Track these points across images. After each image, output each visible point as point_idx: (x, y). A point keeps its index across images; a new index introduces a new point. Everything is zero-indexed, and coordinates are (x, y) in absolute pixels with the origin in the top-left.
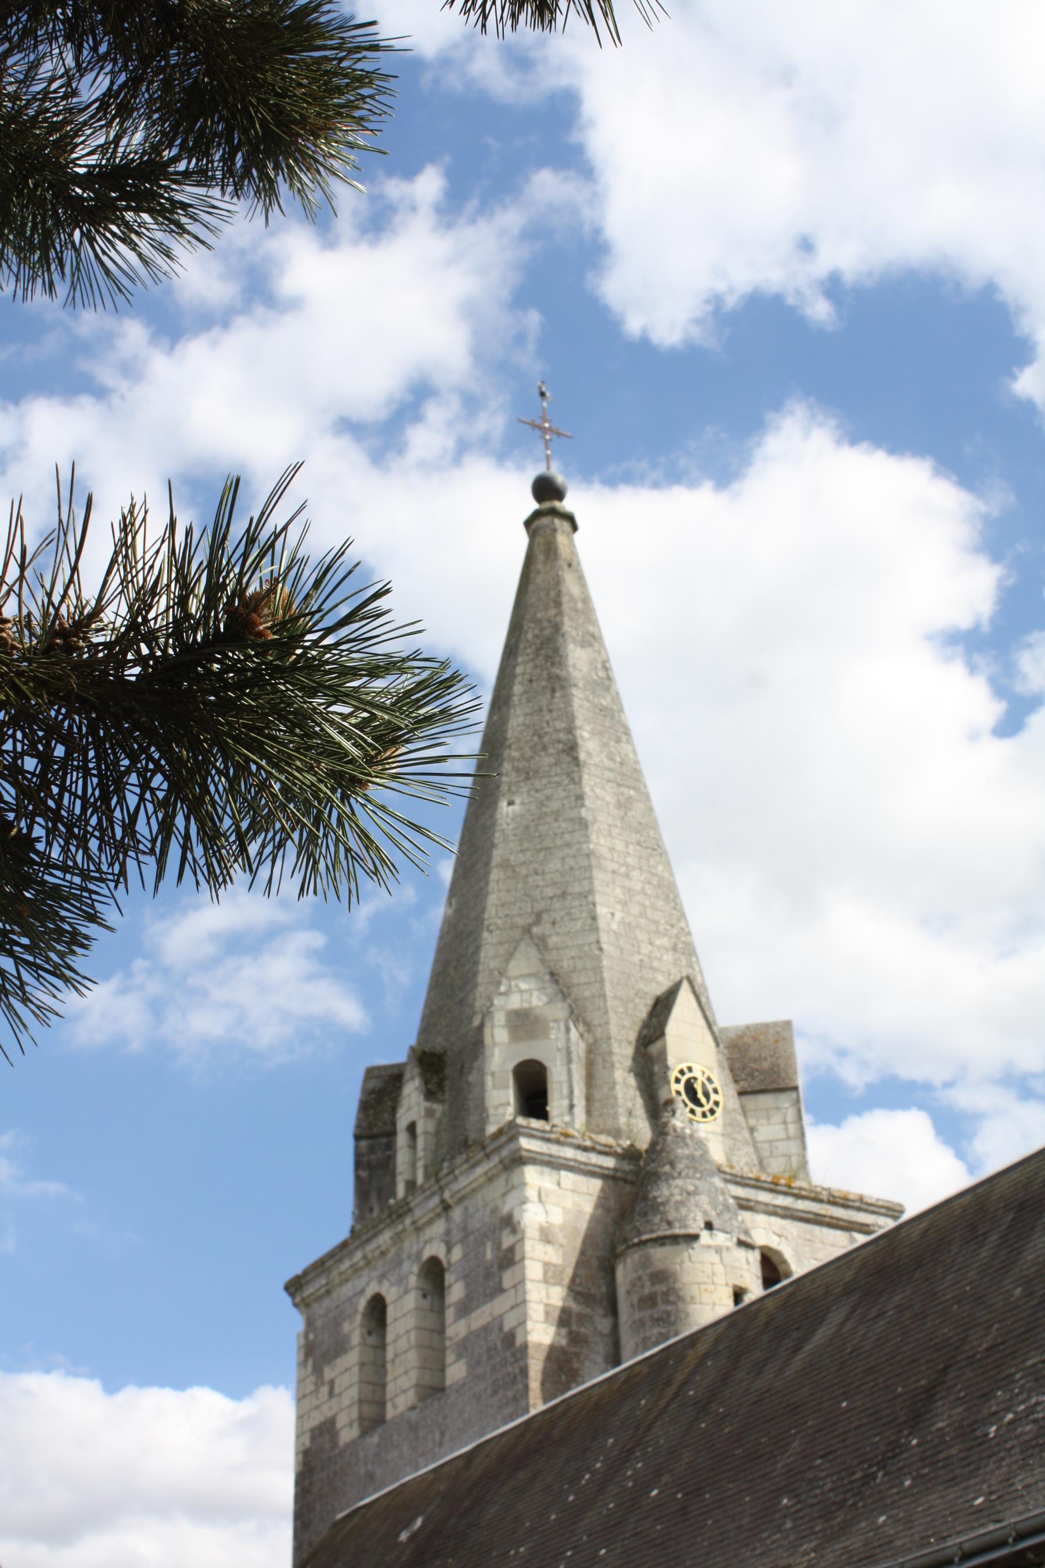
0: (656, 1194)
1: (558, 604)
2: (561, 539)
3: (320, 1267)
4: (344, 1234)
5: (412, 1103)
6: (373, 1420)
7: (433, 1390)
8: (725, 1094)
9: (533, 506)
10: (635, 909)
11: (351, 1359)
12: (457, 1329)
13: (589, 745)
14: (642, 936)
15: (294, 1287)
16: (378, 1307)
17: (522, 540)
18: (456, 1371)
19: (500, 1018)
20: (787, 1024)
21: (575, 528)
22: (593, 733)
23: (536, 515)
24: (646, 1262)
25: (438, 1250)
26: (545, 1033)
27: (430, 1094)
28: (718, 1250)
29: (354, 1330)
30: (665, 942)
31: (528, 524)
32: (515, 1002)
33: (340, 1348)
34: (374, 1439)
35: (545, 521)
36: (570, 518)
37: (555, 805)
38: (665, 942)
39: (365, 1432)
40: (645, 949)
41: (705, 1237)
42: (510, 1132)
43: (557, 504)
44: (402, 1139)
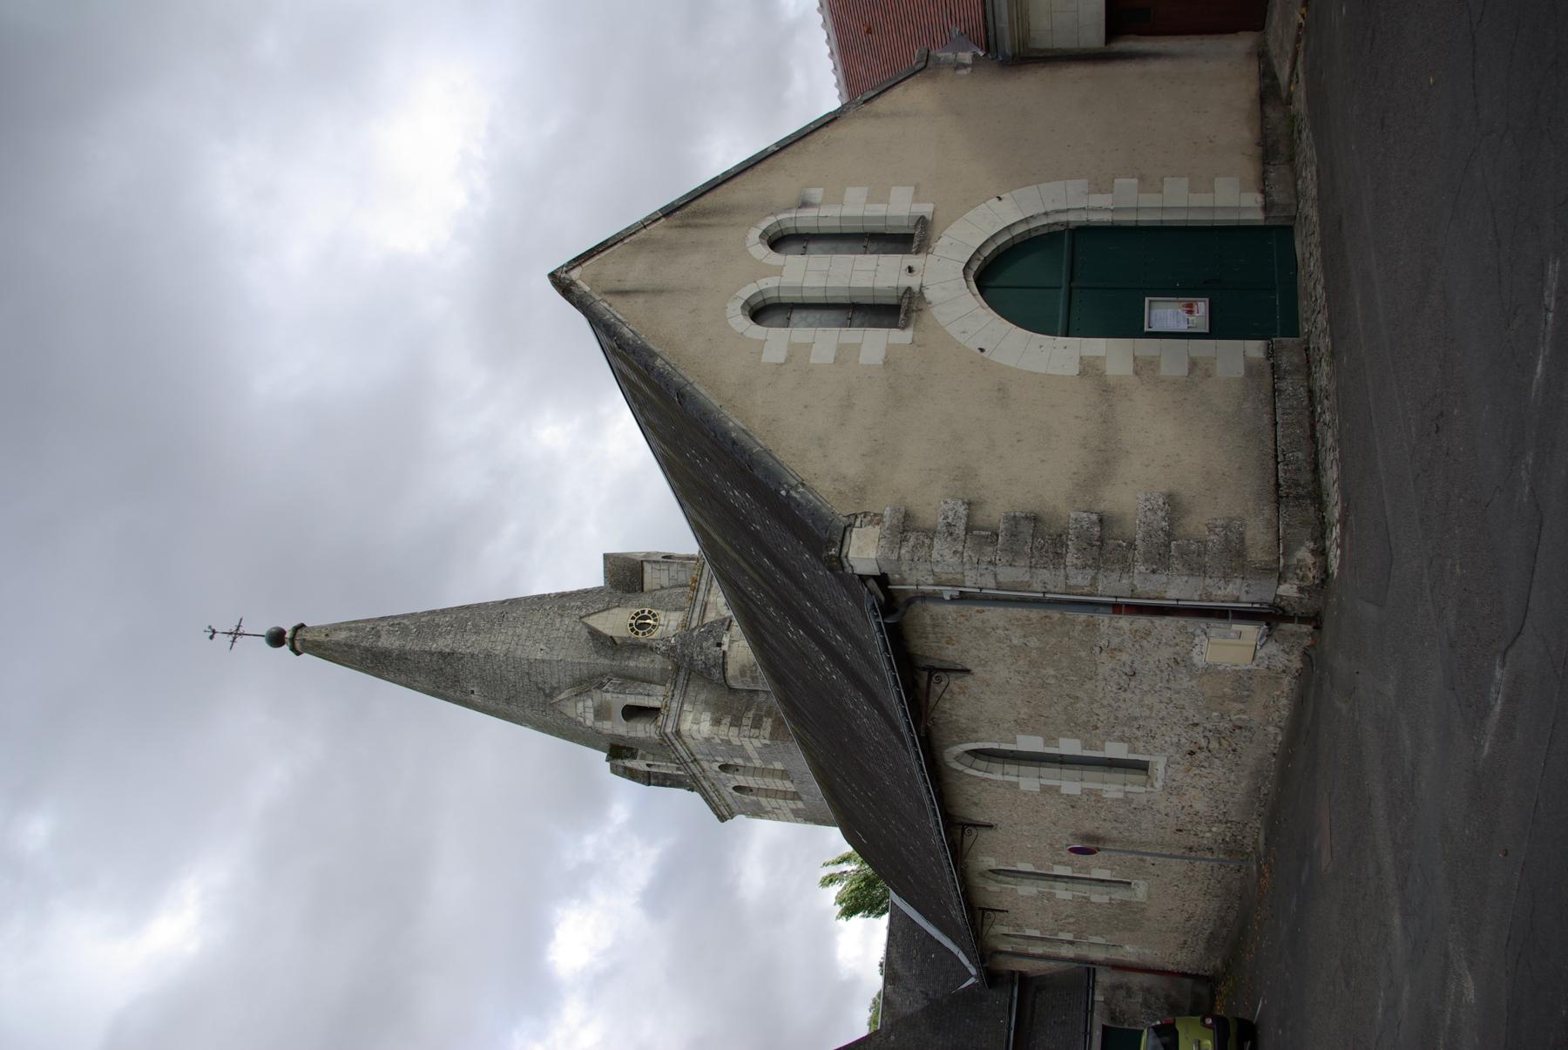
0: (703, 697)
1: (352, 646)
2: (308, 637)
3: (714, 809)
4: (696, 795)
5: (639, 764)
6: (796, 796)
7: (785, 775)
8: (642, 604)
9: (286, 648)
10: (539, 635)
11: (763, 801)
12: (758, 763)
13: (443, 644)
14: (555, 634)
15: (722, 818)
16: (737, 788)
17: (306, 657)
18: (778, 766)
19: (599, 725)
20: (606, 557)
21: (303, 626)
22: (433, 640)
23: (293, 649)
24: (734, 678)
25: (716, 766)
26: (608, 703)
27: (633, 756)
28: (732, 642)
29: (748, 798)
30: (558, 621)
31: (298, 654)
32: (590, 716)
33: (758, 804)
34: (805, 797)
35: (298, 645)
36: (297, 629)
37: (475, 670)
38: (558, 621)
39: (800, 799)
40: (561, 634)
41: (725, 648)
42: (661, 729)
43: (288, 635)
44: (654, 770)
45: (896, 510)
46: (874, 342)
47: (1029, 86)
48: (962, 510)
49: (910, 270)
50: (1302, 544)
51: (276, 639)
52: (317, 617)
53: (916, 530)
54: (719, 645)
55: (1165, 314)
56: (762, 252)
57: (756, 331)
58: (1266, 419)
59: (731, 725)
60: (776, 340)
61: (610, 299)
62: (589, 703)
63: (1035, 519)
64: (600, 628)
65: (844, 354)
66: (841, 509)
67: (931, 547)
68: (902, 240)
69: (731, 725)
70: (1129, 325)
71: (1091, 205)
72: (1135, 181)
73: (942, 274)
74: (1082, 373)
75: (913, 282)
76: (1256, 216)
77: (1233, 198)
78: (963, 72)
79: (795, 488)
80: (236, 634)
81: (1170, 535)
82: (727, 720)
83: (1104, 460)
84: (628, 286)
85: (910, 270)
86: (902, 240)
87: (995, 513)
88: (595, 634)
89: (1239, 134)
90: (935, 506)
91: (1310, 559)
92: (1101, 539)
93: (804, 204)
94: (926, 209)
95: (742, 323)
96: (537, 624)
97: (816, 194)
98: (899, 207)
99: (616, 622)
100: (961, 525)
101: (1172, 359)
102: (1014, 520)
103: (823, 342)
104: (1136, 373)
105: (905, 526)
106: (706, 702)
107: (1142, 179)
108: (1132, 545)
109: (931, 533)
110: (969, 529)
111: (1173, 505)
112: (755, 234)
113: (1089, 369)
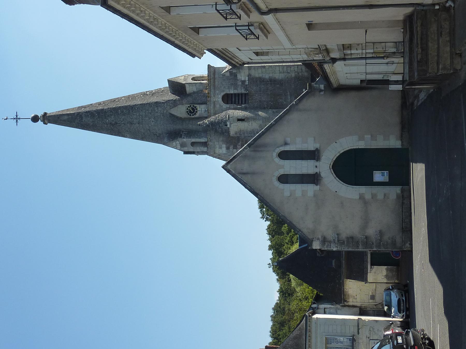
38: (156, 108)
41: (228, 126)
45: (322, 237)
46: (311, 189)
47: (340, 100)
48: (336, 236)
49: (316, 167)
50: (407, 242)
51: (35, 119)
52: (52, 110)
53: (327, 241)
54: (226, 125)
55: (378, 176)
56: (277, 160)
57: (282, 186)
58: (401, 210)
59: (233, 149)
60: (288, 188)
61: (241, 175)
62: (178, 142)
63: (352, 238)
64: (176, 114)
65: (304, 193)
66: (310, 237)
67: (331, 245)
68: (313, 155)
69: (233, 149)
70: (369, 182)
71: (356, 67)
72: (370, 136)
73: (324, 167)
74: (360, 198)
75: (317, 170)
76: (400, 147)
77: (394, 142)
78: (322, 93)
79: (298, 232)
80: (17, 119)
81: (381, 240)
82: (231, 147)
83: (365, 226)
84: (245, 171)
85: (316, 167)
86: (313, 155)
87: (343, 236)
88: (172, 115)
89: (394, 118)
90: (330, 235)
91: (409, 246)
92: (366, 242)
93: (286, 144)
94: (317, 146)
95: (277, 183)
96: (148, 110)
97: (288, 140)
98: (311, 146)
99: (181, 111)
100: (336, 239)
101: (380, 191)
102: (348, 238)
103: (298, 189)
104: (372, 198)
105: (324, 240)
106: (223, 141)
107: (372, 136)
108: (373, 244)
109: (330, 242)
110: (338, 241)
111: (381, 233)
112: (275, 154)
113: (362, 197)
